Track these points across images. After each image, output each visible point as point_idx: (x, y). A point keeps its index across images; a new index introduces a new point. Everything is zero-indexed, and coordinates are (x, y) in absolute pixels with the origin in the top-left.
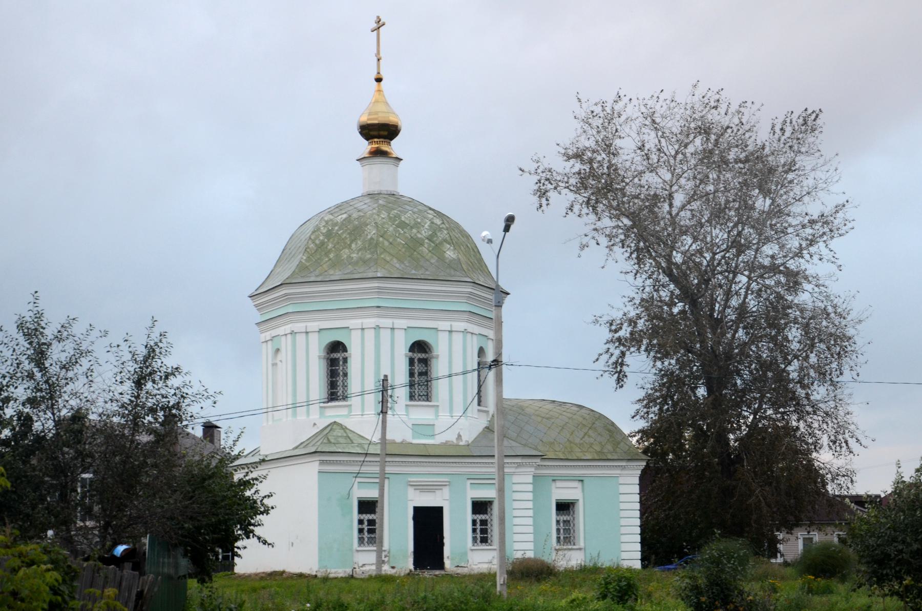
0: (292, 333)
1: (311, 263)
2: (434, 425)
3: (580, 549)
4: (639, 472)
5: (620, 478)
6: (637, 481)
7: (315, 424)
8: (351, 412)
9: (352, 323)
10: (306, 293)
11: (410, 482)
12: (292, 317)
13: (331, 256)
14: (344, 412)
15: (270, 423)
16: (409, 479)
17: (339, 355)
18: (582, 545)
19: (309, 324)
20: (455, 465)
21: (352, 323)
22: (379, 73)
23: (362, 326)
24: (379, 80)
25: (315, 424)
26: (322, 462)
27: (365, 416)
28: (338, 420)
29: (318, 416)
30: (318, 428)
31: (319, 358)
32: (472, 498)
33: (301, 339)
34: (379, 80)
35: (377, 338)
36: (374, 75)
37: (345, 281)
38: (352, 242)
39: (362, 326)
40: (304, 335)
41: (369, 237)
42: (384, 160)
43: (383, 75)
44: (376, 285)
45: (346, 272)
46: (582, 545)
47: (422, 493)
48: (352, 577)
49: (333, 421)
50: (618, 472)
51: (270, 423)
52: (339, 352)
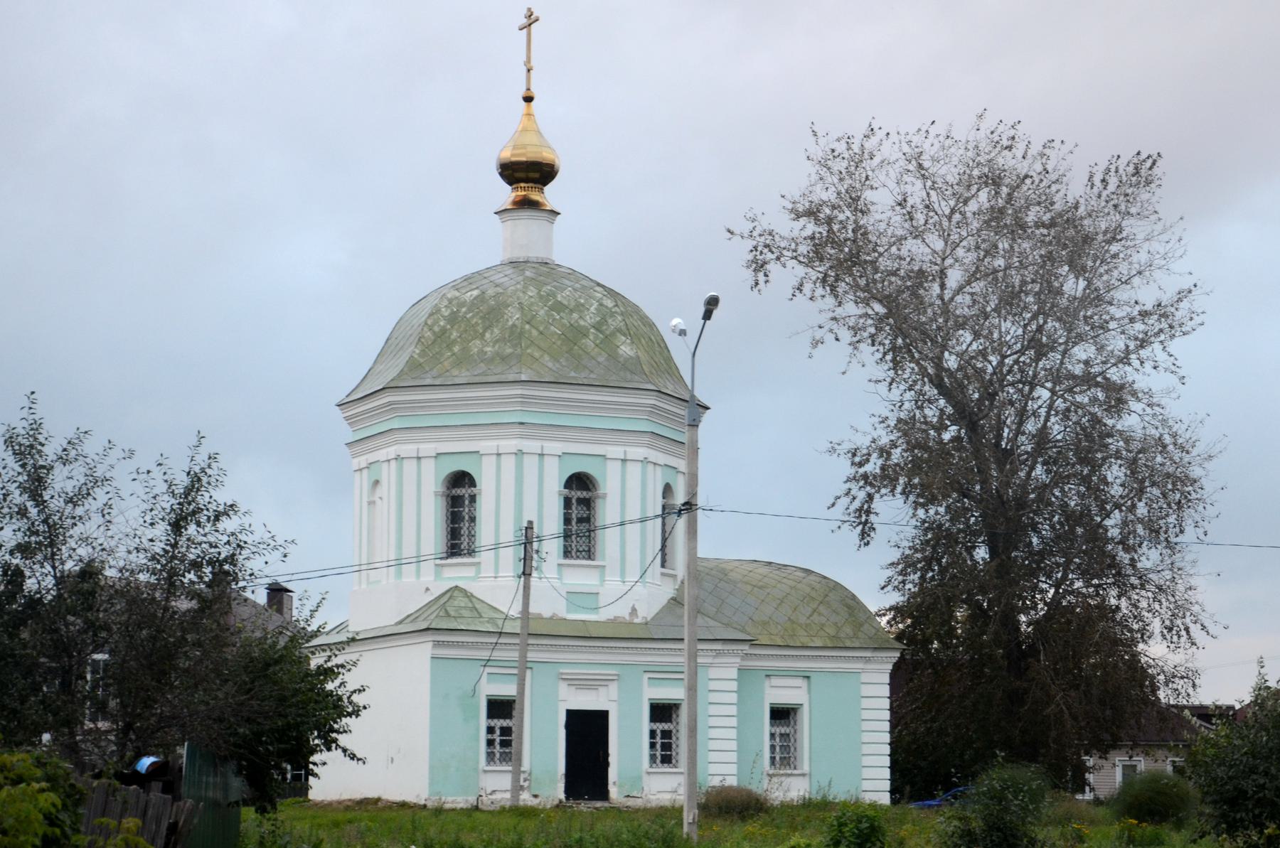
2: (598, 593)
3: (803, 775)
4: (890, 667)
5: (863, 674)
7: (427, 589)
8: (480, 573)
11: (562, 674)
13: (456, 349)
14: (470, 572)
16: (561, 671)
17: (464, 491)
18: (806, 768)
19: (422, 446)
22: (528, 89)
24: (528, 99)
25: (427, 589)
26: (437, 644)
29: (432, 578)
32: (650, 699)
33: (410, 466)
34: (528, 99)
36: (522, 92)
43: (535, 91)
44: (519, 392)
47: (578, 691)
50: (860, 665)
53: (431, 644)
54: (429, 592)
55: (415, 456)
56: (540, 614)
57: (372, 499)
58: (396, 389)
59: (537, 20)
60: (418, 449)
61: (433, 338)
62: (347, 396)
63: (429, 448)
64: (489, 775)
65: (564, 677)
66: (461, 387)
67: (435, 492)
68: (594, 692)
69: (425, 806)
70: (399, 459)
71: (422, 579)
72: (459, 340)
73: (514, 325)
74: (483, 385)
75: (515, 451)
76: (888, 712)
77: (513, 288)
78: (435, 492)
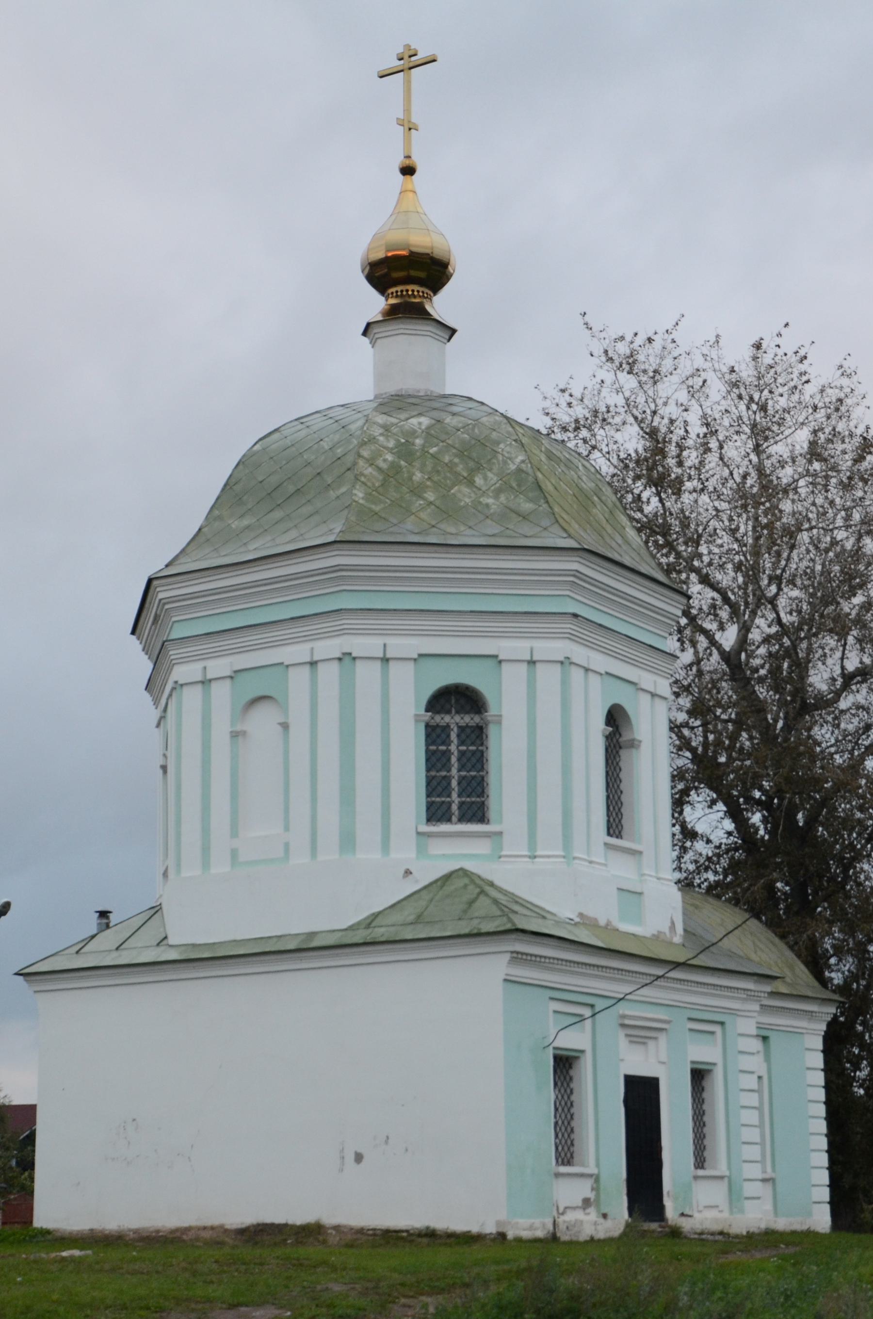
0: (347, 658)
1: (382, 506)
2: (641, 894)
3: (721, 1178)
4: (824, 1027)
5: (806, 1037)
6: (820, 1045)
7: (408, 873)
8: (501, 849)
9: (505, 647)
10: (265, 585)
11: (624, 1017)
12: (348, 622)
13: (430, 496)
14: (482, 847)
15: (220, 867)
16: (628, 1012)
17: (447, 719)
18: (722, 1168)
19: (391, 641)
20: (679, 986)
21: (505, 647)
22: (408, 157)
23: (532, 656)
24: (408, 171)
25: (408, 873)
26: (518, 958)
27: (537, 860)
28: (469, 865)
29: (413, 855)
30: (417, 881)
31: (417, 721)
32: (693, 1062)
33: (329, 674)
34: (408, 171)
35: (565, 683)
36: (399, 160)
37: (530, 552)
38: (472, 472)
39: (532, 656)
40: (307, 669)
41: (513, 467)
42: (438, 332)
43: (418, 160)
44: (575, 566)
45: (489, 533)
46: (722, 1168)
47: (634, 1046)
48: (554, 1238)
49: (457, 867)
50: (804, 1024)
51: (220, 867)
52: (448, 712)
53: (508, 956)
54: (410, 877)
55: (308, 659)
56: (596, 919)
57: (239, 728)
58: (358, 546)
59: (434, 61)
60: (312, 649)
61: (381, 478)
62: (167, 566)
63: (219, 667)
64: (562, 1181)
65: (627, 1022)
66: (475, 550)
67: (416, 715)
68: (641, 1048)
69: (502, 1236)
70: (347, 660)
71: (393, 855)
72: (428, 483)
73: (519, 470)
74: (547, 552)
75: (562, 659)
76: (823, 1091)
77: (316, 446)
78: (416, 715)
